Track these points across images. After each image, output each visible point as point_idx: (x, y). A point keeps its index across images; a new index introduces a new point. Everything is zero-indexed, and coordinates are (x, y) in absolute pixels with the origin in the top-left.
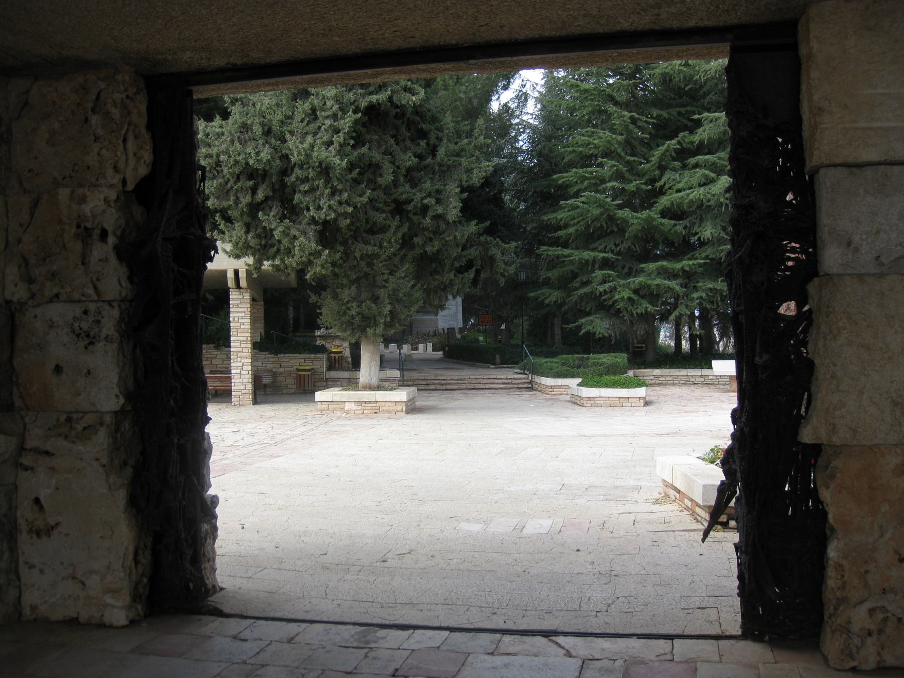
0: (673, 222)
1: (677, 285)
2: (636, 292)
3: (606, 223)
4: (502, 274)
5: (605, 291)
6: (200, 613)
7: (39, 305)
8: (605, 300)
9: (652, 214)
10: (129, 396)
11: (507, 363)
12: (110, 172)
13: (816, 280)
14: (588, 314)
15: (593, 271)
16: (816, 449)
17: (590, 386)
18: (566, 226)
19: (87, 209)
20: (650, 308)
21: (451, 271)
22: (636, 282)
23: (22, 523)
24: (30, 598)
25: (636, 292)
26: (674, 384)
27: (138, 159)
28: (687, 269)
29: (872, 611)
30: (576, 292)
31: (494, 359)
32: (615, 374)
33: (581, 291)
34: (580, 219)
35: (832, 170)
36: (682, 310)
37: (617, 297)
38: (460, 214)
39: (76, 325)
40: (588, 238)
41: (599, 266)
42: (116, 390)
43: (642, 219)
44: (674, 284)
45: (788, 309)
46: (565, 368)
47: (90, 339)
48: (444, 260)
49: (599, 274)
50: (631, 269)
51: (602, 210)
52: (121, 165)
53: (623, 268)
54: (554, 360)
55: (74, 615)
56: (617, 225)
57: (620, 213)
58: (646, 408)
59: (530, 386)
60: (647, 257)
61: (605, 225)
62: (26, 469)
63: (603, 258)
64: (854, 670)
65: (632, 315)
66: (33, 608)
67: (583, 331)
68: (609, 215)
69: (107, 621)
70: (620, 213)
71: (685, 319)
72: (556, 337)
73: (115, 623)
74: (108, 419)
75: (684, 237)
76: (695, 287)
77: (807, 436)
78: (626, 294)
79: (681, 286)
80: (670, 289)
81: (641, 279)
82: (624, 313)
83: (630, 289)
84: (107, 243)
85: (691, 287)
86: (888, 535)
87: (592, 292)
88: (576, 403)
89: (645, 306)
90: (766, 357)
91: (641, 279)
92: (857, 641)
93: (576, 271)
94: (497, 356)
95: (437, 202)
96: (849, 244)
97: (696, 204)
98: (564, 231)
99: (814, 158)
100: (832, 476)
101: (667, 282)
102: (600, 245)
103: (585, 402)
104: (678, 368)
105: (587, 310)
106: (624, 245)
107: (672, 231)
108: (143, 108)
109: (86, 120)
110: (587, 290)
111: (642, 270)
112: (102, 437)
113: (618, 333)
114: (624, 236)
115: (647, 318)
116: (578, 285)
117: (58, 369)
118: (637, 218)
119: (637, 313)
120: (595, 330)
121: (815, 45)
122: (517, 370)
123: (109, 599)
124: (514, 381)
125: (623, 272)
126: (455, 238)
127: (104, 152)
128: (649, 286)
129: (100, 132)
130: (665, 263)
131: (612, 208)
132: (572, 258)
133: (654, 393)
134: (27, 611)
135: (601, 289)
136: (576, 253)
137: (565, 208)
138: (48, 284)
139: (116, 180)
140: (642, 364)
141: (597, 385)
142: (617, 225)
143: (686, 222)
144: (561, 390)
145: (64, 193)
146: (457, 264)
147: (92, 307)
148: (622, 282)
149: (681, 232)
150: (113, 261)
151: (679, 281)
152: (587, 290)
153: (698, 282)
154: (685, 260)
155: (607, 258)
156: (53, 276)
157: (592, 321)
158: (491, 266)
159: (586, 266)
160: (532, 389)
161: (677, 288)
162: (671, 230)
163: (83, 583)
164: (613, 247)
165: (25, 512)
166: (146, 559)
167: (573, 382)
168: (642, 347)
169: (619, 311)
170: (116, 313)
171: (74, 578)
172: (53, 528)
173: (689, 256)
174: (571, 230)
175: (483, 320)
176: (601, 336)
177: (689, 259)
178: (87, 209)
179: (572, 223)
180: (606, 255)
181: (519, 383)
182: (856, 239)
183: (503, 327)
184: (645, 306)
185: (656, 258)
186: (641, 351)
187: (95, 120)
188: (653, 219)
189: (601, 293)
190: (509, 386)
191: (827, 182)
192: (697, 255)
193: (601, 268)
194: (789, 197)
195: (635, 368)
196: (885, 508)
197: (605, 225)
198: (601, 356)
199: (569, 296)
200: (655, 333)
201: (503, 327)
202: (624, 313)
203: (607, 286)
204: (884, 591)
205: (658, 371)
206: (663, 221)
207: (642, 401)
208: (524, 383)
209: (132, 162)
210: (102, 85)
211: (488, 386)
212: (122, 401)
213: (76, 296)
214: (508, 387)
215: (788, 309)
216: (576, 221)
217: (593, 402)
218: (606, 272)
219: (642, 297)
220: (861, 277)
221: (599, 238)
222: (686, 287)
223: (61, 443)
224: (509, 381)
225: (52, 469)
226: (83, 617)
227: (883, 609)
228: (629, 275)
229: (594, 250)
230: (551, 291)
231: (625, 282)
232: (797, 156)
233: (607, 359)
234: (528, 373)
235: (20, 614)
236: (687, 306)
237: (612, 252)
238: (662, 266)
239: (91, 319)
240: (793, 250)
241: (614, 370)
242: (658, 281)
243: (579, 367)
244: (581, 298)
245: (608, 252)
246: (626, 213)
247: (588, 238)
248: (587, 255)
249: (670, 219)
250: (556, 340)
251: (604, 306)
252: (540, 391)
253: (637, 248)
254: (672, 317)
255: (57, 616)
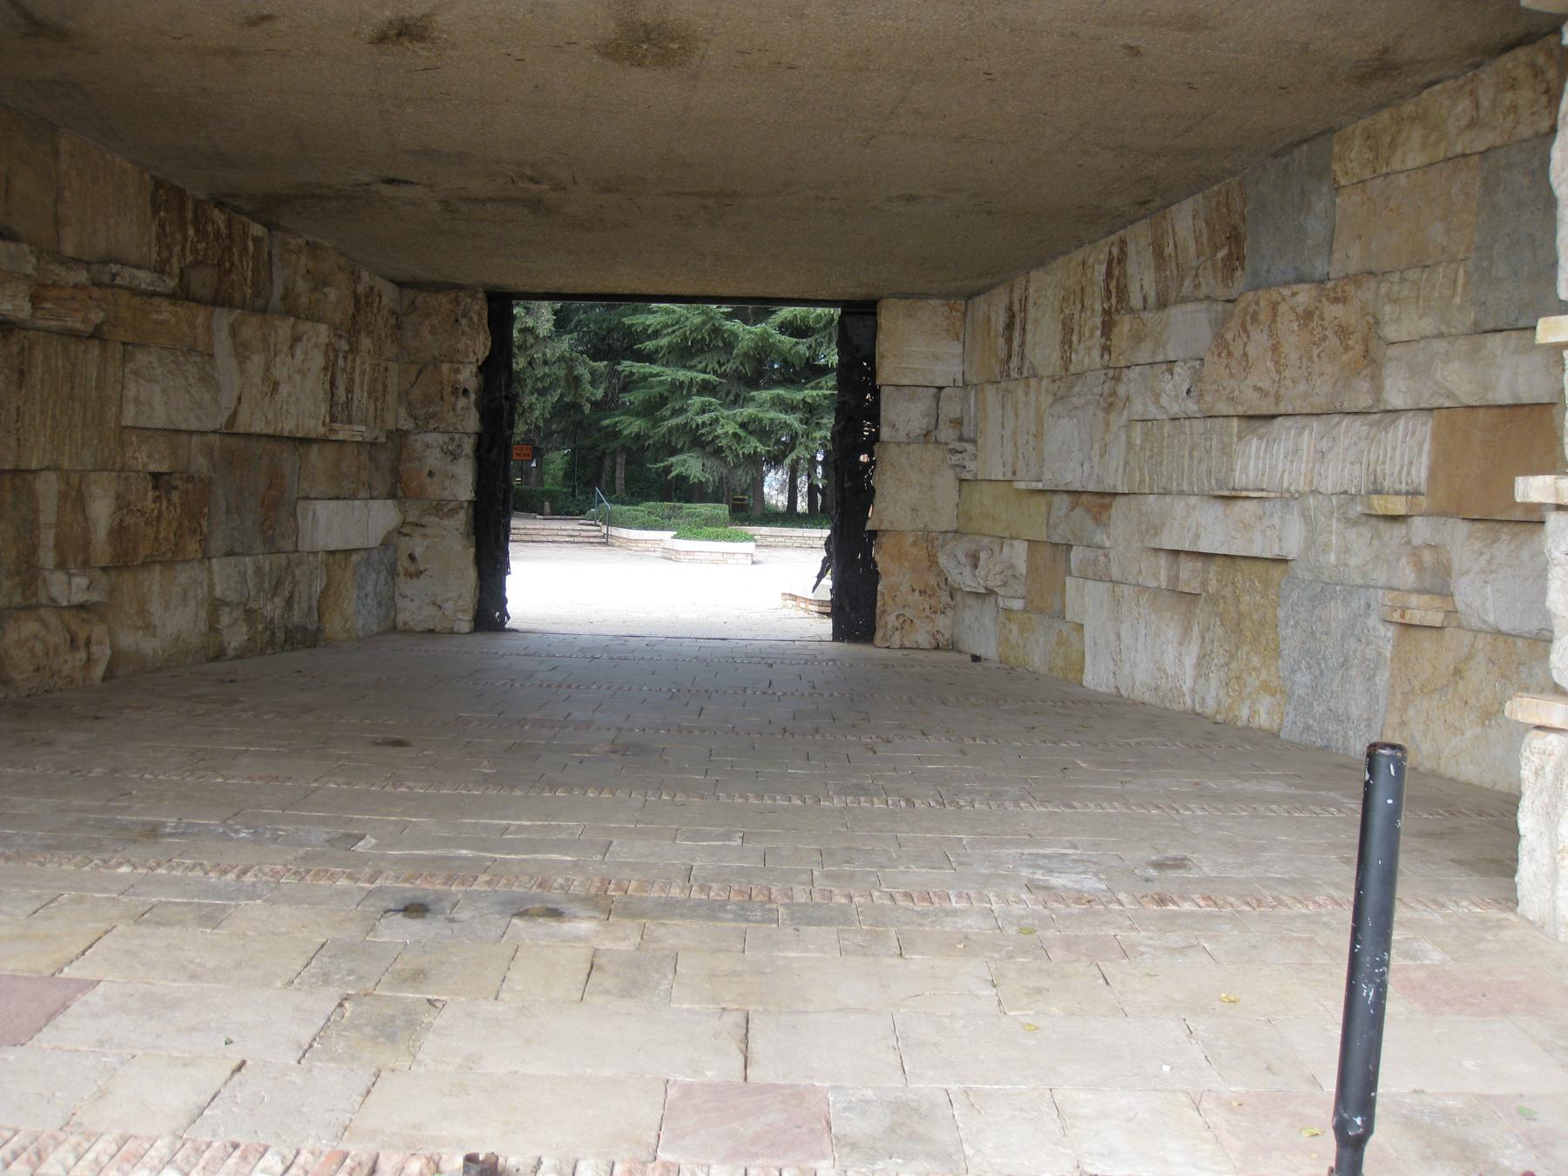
0: (794, 340)
1: (796, 420)
2: (743, 425)
3: (709, 335)
4: (588, 400)
5: (704, 423)
6: (499, 631)
7: (420, 433)
8: (702, 435)
9: (767, 327)
10: (477, 492)
11: (559, 514)
12: (471, 354)
13: (878, 444)
14: (681, 451)
15: (689, 396)
16: (874, 534)
17: (689, 538)
18: (657, 334)
19: (461, 377)
20: (761, 448)
21: (532, 394)
22: (745, 414)
23: (401, 570)
24: (403, 617)
25: (743, 425)
26: (786, 547)
27: (486, 347)
28: (809, 401)
29: (898, 617)
30: (665, 423)
31: (542, 508)
32: (711, 526)
33: (673, 422)
34: (676, 327)
35: (887, 388)
36: (800, 452)
37: (719, 431)
38: (553, 329)
39: (445, 447)
40: (684, 352)
41: (698, 391)
42: (471, 488)
43: (756, 334)
44: (792, 419)
45: (864, 458)
46: (653, 517)
47: (455, 457)
48: (525, 380)
49: (697, 401)
50: (737, 396)
51: (704, 318)
52: (476, 350)
53: (728, 394)
54: (639, 508)
55: (431, 627)
56: (723, 339)
57: (728, 325)
58: (754, 566)
59: (604, 540)
60: (753, 382)
61: (707, 337)
62: (406, 535)
63: (703, 380)
64: (888, 647)
65: (737, 455)
66: (405, 623)
67: (674, 474)
68: (714, 325)
69: (456, 630)
70: (728, 325)
71: (804, 464)
72: (617, 482)
73: (462, 631)
74: (466, 505)
75: (808, 359)
76: (818, 424)
77: (869, 526)
78: (731, 428)
79: (801, 421)
80: (786, 425)
81: (750, 410)
82: (727, 452)
83: (736, 422)
84: (469, 397)
85: (814, 424)
86: (907, 577)
87: (686, 423)
88: (671, 559)
89: (754, 445)
90: (850, 484)
91: (749, 411)
92: (890, 633)
93: (666, 394)
94: (547, 504)
95: (527, 314)
96: (894, 426)
97: (825, 319)
98: (654, 342)
99: (879, 382)
100: (881, 548)
101: (783, 416)
102: (700, 363)
103: (682, 557)
104: (793, 526)
105: (679, 446)
106: (730, 364)
107: (793, 352)
108: (486, 313)
109: (457, 321)
110: (680, 420)
111: (752, 399)
112: (462, 517)
113: (717, 479)
114: (731, 354)
115: (754, 460)
116: (668, 413)
117: (431, 474)
118: (750, 333)
119: (743, 453)
120: (688, 472)
121: (883, 321)
122: (581, 521)
123: (460, 616)
124: (583, 534)
125: (728, 400)
126: (544, 354)
127: (469, 343)
128: (761, 420)
129: (467, 329)
130: (781, 392)
131: (718, 316)
132: (662, 378)
133: (762, 554)
134: (400, 625)
135: (699, 420)
136: (668, 371)
137: (657, 311)
138: (431, 421)
139: (474, 360)
140: (746, 521)
141: (696, 537)
142: (723, 339)
143: (811, 340)
144: (648, 545)
145: (445, 367)
146: (540, 385)
147: (457, 436)
148: (726, 413)
149: (805, 354)
150: (473, 410)
151: (799, 415)
152: (680, 420)
153: (822, 418)
154: (807, 389)
155: (709, 381)
156: (433, 416)
157: (685, 461)
158: (576, 388)
159: (677, 387)
160: (606, 544)
161: (796, 424)
162: (791, 349)
163: (440, 607)
164: (717, 367)
165: (403, 562)
166: (478, 594)
167: (666, 535)
168: (743, 500)
169: (719, 450)
170: (471, 441)
171: (434, 604)
172: (421, 572)
173: (812, 384)
174: (664, 342)
175: (518, 452)
176: (696, 480)
177: (812, 388)
178: (461, 377)
179: (665, 332)
180: (707, 377)
181: (589, 537)
182: (897, 424)
183: (534, 465)
184: (754, 445)
185: (772, 384)
186: (742, 505)
187: (464, 322)
188: (771, 335)
189: (698, 425)
190: (576, 539)
191: (885, 392)
192: (823, 383)
193: (699, 394)
194: (868, 396)
195: (737, 525)
196: (906, 563)
197: (707, 337)
198: (698, 505)
199: (654, 427)
200: (758, 483)
201: (534, 465)
202: (727, 452)
203: (706, 417)
204: (904, 606)
205: (765, 529)
206: (783, 338)
207: (750, 558)
208: (595, 537)
209: (482, 349)
210: (469, 300)
211: (550, 539)
212: (473, 494)
213: (451, 429)
214: (574, 541)
215: (864, 458)
216: (670, 330)
217: (691, 557)
218: (706, 399)
219: (751, 433)
220: (899, 444)
221: (701, 351)
222: (806, 423)
223: (434, 519)
224: (577, 533)
225: (425, 536)
226: (439, 628)
227: (903, 615)
228: (735, 403)
229: (691, 368)
230: (632, 419)
231: (730, 413)
232: (873, 374)
233: (704, 509)
234: (600, 524)
235: (395, 628)
236: (807, 448)
237: (715, 372)
238: (779, 395)
239: (455, 443)
240: (868, 426)
241: (711, 521)
242: (772, 414)
243: (669, 518)
244: (670, 430)
245: (709, 373)
246: (736, 325)
247: (684, 352)
248: (682, 375)
249: (790, 336)
250: (617, 486)
251: (698, 440)
252: (620, 546)
253: (748, 370)
254: (788, 461)
255: (420, 628)
